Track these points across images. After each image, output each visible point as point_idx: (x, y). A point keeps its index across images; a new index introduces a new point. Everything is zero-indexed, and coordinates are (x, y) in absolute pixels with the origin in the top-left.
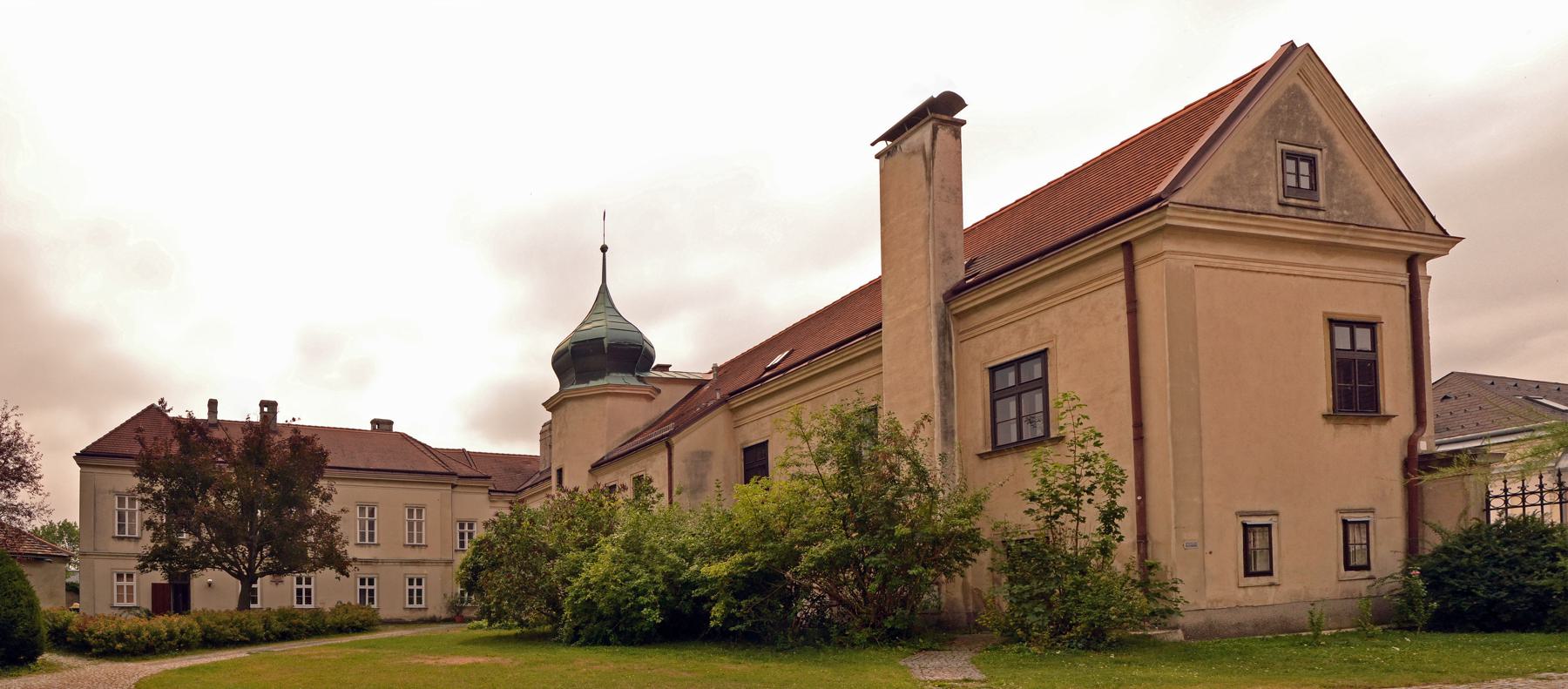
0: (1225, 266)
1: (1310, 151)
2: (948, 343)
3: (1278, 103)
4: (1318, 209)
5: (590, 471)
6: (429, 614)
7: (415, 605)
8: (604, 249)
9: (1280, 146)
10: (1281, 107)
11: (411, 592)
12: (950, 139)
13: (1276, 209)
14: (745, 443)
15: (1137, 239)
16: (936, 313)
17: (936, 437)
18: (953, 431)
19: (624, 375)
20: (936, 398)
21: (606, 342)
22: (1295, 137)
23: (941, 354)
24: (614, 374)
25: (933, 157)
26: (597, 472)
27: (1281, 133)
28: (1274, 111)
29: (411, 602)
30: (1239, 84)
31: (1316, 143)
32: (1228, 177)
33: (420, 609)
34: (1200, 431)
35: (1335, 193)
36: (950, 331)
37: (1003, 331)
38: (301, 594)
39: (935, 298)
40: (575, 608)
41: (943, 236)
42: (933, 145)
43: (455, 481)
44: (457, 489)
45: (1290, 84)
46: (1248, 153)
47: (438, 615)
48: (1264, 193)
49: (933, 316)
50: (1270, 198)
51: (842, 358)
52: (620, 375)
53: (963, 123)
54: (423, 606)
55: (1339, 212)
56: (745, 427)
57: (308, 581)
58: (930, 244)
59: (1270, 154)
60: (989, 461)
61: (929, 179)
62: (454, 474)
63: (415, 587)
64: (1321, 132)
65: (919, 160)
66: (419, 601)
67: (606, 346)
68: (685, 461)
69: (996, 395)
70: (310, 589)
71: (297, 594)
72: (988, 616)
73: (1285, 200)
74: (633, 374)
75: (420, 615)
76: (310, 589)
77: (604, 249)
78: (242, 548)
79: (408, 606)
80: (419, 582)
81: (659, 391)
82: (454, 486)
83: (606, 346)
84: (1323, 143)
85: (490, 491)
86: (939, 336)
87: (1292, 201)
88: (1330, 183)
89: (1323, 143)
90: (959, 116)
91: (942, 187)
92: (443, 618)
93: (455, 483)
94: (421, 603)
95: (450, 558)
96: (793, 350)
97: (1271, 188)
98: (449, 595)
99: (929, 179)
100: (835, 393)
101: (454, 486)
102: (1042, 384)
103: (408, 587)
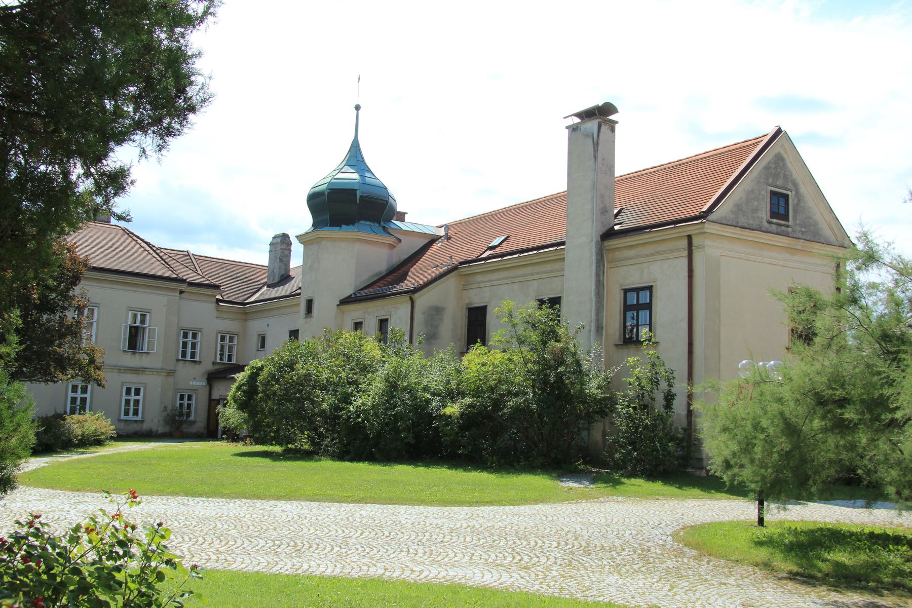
0: (737, 256)
1: (785, 192)
2: (602, 268)
3: (769, 163)
4: (788, 226)
5: (338, 305)
6: (145, 427)
7: (131, 417)
8: (358, 108)
9: (770, 188)
10: (771, 165)
11: (128, 402)
12: (609, 132)
13: (765, 224)
14: (470, 303)
15: (693, 234)
16: (596, 247)
17: (592, 329)
18: (602, 327)
19: (371, 223)
20: (594, 304)
21: (358, 194)
22: (778, 183)
23: (598, 275)
24: (363, 222)
25: (598, 144)
26: (342, 307)
27: (770, 180)
28: (767, 168)
29: (127, 413)
30: (757, 140)
31: (789, 187)
32: (741, 204)
33: (136, 421)
34: (719, 352)
35: (798, 218)
36: (604, 260)
37: (631, 267)
38: (134, 410)
39: (596, 237)
40: (95, 414)
41: (602, 196)
42: (598, 135)
43: (184, 287)
44: (183, 295)
45: (777, 152)
46: (752, 191)
47: (154, 428)
48: (760, 215)
49: (594, 249)
50: (762, 218)
51: (541, 258)
52: (368, 223)
53: (617, 122)
54: (139, 417)
55: (799, 229)
56: (470, 291)
57: (84, 390)
58: (595, 200)
59: (763, 192)
60: (621, 350)
61: (595, 157)
62: (182, 281)
63: (132, 397)
64: (792, 181)
65: (590, 141)
66: (136, 413)
67: (358, 197)
68: (424, 313)
69: (627, 308)
70: (86, 398)
71: (72, 403)
72: (664, 455)
73: (771, 220)
74: (379, 223)
75: (136, 427)
76: (86, 398)
77: (358, 108)
78: (553, 455)
79: (123, 417)
80: (137, 392)
81: (400, 241)
82: (181, 292)
83: (358, 197)
84: (793, 188)
85: (218, 301)
86: (597, 263)
87: (775, 220)
88: (795, 211)
89: (793, 188)
90: (612, 117)
91: (603, 164)
92: (159, 432)
93: (183, 289)
94: (137, 415)
95: (172, 368)
96: (508, 237)
97: (763, 212)
98: (170, 408)
99: (595, 157)
100: (535, 281)
101: (181, 292)
102: (649, 306)
103: (125, 397)
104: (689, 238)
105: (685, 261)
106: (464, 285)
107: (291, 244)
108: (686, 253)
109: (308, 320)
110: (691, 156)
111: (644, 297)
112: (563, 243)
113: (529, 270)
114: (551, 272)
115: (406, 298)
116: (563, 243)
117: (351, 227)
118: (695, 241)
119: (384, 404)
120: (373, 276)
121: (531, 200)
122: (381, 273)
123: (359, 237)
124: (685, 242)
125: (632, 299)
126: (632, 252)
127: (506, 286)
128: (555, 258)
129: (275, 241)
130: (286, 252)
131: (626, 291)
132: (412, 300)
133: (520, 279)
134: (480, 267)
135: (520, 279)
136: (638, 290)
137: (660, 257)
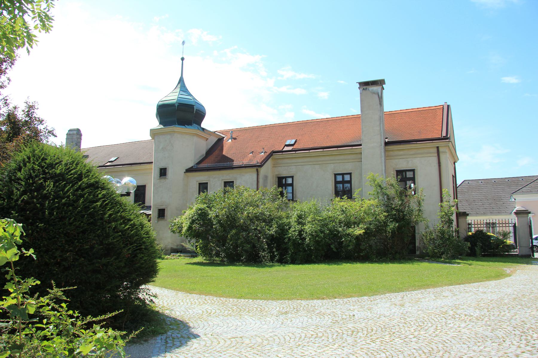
5: (185, 172)
8: (183, 59)
37: (401, 160)
67: (195, 110)
77: (183, 59)
100: (332, 164)
104: (438, 148)
105: (435, 159)
106: (274, 164)
107: (82, 135)
108: (436, 155)
109: (163, 180)
110: (415, 108)
111: (347, 178)
112: (360, 145)
113: (327, 158)
114: (345, 159)
115: (254, 169)
116: (360, 145)
117: (190, 126)
118: (441, 149)
119: (375, 229)
120: (201, 157)
121: (278, 123)
122: (203, 155)
123: (197, 133)
124: (436, 150)
125: (339, 178)
126: (401, 153)
127: (309, 166)
128: (350, 153)
129: (71, 133)
130: (80, 140)
131: (336, 175)
132: (257, 170)
133: (320, 163)
134: (315, 153)
135: (320, 163)
136: (343, 174)
137: (420, 156)
